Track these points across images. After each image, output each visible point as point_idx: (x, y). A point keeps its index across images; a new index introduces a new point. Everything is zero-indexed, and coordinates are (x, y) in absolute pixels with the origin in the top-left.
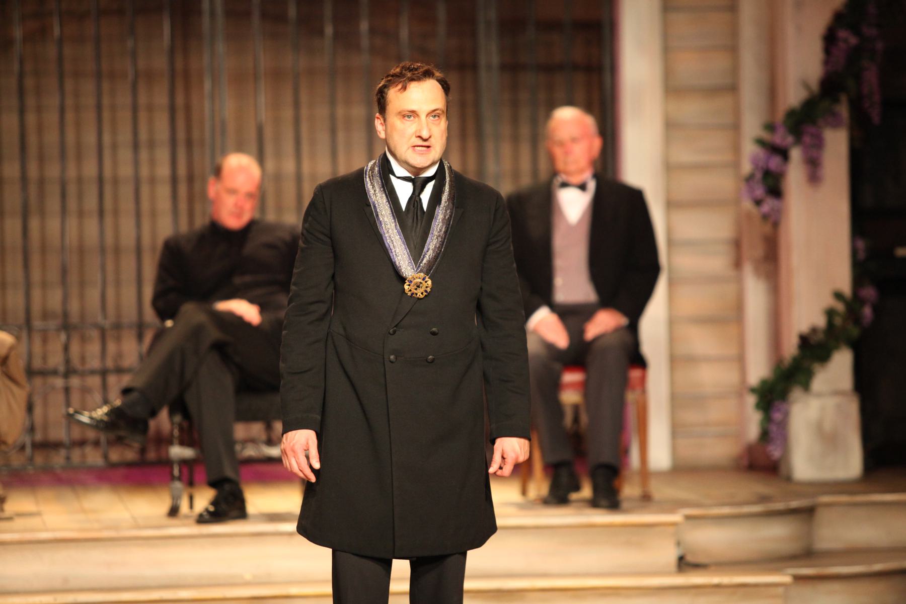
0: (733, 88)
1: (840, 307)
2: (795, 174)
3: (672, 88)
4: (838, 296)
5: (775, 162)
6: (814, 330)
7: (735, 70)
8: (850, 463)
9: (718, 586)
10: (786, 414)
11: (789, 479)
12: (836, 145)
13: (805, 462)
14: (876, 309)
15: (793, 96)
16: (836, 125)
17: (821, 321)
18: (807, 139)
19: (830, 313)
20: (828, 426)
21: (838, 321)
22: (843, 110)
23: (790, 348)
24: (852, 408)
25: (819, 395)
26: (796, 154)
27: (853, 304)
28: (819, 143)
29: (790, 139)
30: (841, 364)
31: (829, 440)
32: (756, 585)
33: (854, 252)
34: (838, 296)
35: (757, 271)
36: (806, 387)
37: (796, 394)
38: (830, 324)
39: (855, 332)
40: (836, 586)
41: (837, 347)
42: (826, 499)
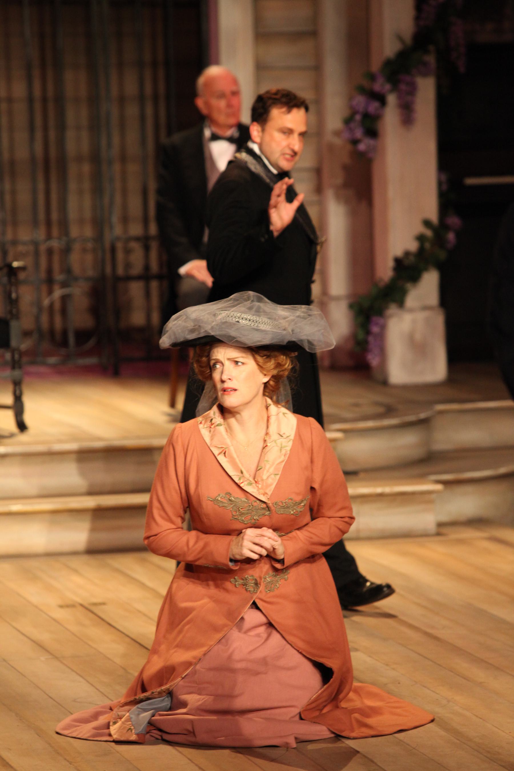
0: (313, 33)
1: (429, 233)
2: (390, 117)
3: (262, 34)
4: (427, 223)
5: (373, 106)
6: (407, 254)
7: (315, 18)
8: (437, 369)
9: (381, 496)
10: (383, 327)
11: (385, 383)
12: (426, 92)
13: (399, 369)
14: (458, 235)
15: (388, 47)
16: (425, 75)
17: (413, 246)
18: (403, 87)
19: (421, 238)
20: (418, 337)
21: (427, 245)
22: (431, 59)
23: (385, 271)
24: (439, 320)
25: (411, 310)
26: (392, 99)
27: (439, 229)
28: (412, 90)
29: (388, 87)
30: (429, 284)
31: (418, 349)
32: (413, 493)
33: (440, 184)
34: (427, 223)
35: (338, 197)
36: (401, 304)
37: (392, 310)
38: (421, 250)
39: (442, 255)
40: (469, 488)
41: (426, 269)
42: (440, 407)
